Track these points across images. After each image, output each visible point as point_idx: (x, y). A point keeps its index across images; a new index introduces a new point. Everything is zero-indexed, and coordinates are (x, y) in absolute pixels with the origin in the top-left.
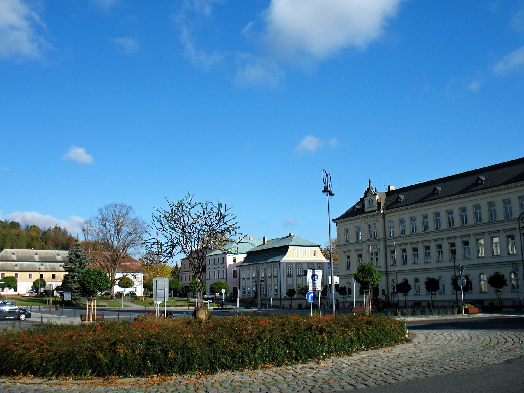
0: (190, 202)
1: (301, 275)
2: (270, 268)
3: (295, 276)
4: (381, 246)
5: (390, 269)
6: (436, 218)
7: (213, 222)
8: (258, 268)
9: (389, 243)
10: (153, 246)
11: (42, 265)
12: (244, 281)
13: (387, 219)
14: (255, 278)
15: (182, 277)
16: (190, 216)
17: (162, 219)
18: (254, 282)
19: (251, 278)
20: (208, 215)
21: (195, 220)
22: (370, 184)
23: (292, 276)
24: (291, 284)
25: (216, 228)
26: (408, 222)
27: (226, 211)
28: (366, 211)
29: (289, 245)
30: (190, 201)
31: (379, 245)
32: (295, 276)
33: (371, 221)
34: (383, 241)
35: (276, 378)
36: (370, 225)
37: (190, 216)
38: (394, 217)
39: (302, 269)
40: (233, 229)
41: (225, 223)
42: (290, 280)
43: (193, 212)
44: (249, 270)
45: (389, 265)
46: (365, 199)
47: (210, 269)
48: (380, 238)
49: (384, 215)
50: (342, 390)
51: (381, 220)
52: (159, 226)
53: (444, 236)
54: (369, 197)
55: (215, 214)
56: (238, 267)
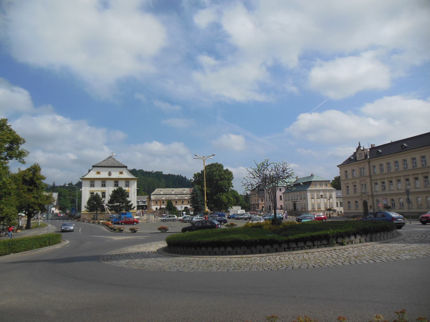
0: (267, 162)
1: (319, 197)
2: (305, 193)
3: (316, 198)
4: (368, 180)
5: (374, 193)
6: (404, 163)
7: (280, 172)
8: (304, 193)
9: (373, 178)
10: (249, 187)
11: (176, 196)
12: (286, 202)
13: (371, 164)
14: (292, 200)
15: (251, 200)
16: (267, 170)
17: (253, 172)
18: (292, 202)
19: (290, 200)
20: (267, 166)
21: (270, 172)
22: (359, 144)
23: (314, 198)
24: (314, 203)
25: (283, 176)
26: (385, 167)
27: (204, 162)
28: (358, 160)
29: (312, 180)
30: (267, 162)
31: (367, 179)
32: (316, 198)
33: (362, 166)
34: (369, 177)
35: (371, 257)
36: (361, 169)
37: (267, 170)
38: (376, 163)
39: (320, 194)
40: (291, 176)
41: (287, 173)
42: (313, 200)
43: (269, 168)
44: (301, 194)
45: (374, 191)
46: (357, 153)
47: (267, 195)
48: (367, 175)
49: (369, 162)
50: (367, 262)
51: (367, 165)
52: (252, 176)
53: (410, 173)
54: (359, 152)
55: (281, 169)
56: (283, 194)
